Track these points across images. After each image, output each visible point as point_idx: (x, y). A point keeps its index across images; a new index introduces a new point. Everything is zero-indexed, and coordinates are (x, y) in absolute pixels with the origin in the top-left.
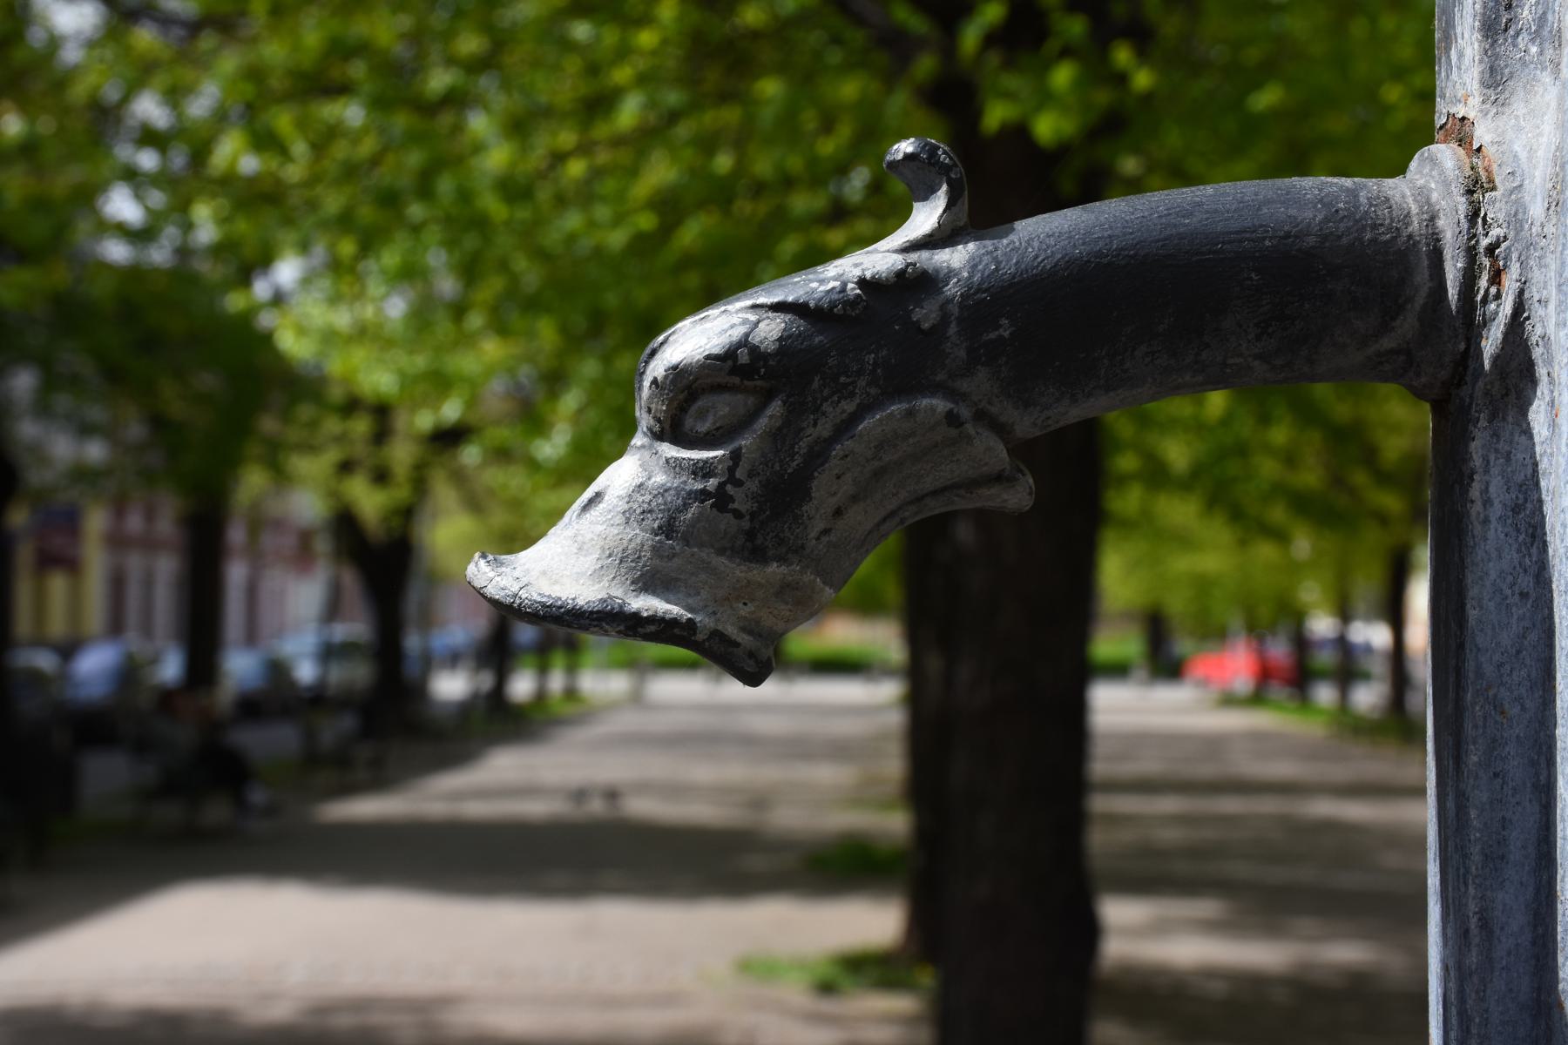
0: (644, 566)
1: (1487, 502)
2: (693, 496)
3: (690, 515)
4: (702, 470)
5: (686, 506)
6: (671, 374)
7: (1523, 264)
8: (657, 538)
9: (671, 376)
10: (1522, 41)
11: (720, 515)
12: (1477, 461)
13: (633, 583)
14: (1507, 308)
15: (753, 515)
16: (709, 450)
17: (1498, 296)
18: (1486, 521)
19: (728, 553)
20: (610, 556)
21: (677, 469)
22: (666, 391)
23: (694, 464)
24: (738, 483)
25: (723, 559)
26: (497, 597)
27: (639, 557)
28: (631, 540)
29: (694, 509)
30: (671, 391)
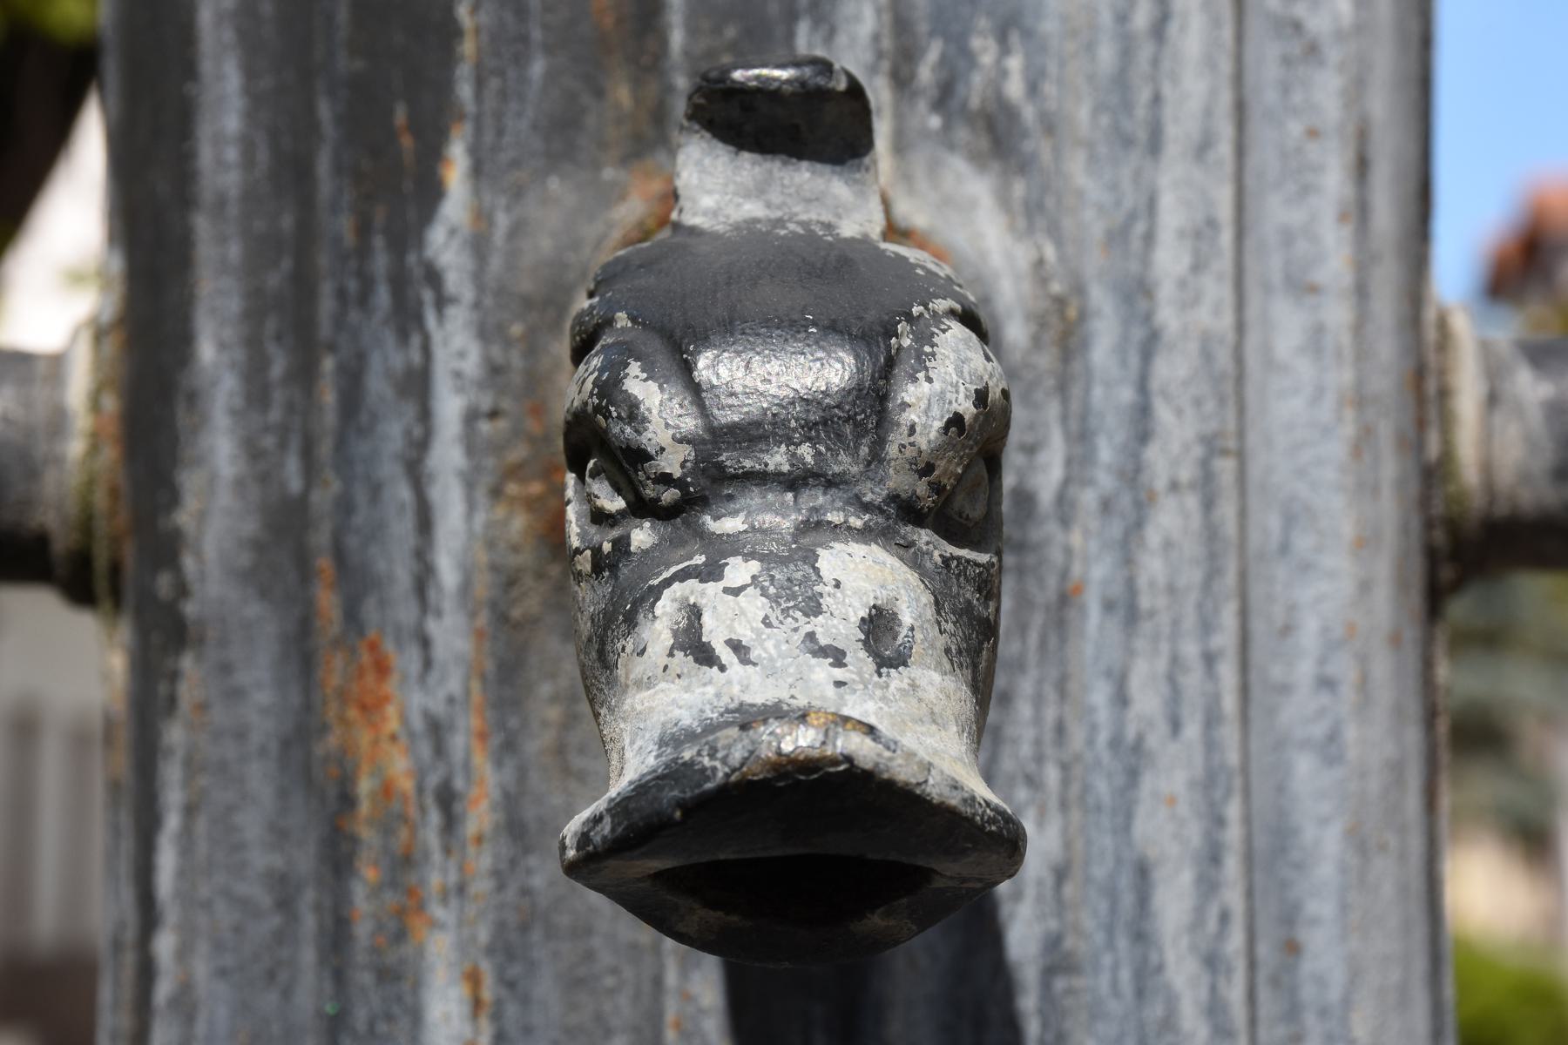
21: (962, 579)
22: (971, 442)
23: (981, 573)
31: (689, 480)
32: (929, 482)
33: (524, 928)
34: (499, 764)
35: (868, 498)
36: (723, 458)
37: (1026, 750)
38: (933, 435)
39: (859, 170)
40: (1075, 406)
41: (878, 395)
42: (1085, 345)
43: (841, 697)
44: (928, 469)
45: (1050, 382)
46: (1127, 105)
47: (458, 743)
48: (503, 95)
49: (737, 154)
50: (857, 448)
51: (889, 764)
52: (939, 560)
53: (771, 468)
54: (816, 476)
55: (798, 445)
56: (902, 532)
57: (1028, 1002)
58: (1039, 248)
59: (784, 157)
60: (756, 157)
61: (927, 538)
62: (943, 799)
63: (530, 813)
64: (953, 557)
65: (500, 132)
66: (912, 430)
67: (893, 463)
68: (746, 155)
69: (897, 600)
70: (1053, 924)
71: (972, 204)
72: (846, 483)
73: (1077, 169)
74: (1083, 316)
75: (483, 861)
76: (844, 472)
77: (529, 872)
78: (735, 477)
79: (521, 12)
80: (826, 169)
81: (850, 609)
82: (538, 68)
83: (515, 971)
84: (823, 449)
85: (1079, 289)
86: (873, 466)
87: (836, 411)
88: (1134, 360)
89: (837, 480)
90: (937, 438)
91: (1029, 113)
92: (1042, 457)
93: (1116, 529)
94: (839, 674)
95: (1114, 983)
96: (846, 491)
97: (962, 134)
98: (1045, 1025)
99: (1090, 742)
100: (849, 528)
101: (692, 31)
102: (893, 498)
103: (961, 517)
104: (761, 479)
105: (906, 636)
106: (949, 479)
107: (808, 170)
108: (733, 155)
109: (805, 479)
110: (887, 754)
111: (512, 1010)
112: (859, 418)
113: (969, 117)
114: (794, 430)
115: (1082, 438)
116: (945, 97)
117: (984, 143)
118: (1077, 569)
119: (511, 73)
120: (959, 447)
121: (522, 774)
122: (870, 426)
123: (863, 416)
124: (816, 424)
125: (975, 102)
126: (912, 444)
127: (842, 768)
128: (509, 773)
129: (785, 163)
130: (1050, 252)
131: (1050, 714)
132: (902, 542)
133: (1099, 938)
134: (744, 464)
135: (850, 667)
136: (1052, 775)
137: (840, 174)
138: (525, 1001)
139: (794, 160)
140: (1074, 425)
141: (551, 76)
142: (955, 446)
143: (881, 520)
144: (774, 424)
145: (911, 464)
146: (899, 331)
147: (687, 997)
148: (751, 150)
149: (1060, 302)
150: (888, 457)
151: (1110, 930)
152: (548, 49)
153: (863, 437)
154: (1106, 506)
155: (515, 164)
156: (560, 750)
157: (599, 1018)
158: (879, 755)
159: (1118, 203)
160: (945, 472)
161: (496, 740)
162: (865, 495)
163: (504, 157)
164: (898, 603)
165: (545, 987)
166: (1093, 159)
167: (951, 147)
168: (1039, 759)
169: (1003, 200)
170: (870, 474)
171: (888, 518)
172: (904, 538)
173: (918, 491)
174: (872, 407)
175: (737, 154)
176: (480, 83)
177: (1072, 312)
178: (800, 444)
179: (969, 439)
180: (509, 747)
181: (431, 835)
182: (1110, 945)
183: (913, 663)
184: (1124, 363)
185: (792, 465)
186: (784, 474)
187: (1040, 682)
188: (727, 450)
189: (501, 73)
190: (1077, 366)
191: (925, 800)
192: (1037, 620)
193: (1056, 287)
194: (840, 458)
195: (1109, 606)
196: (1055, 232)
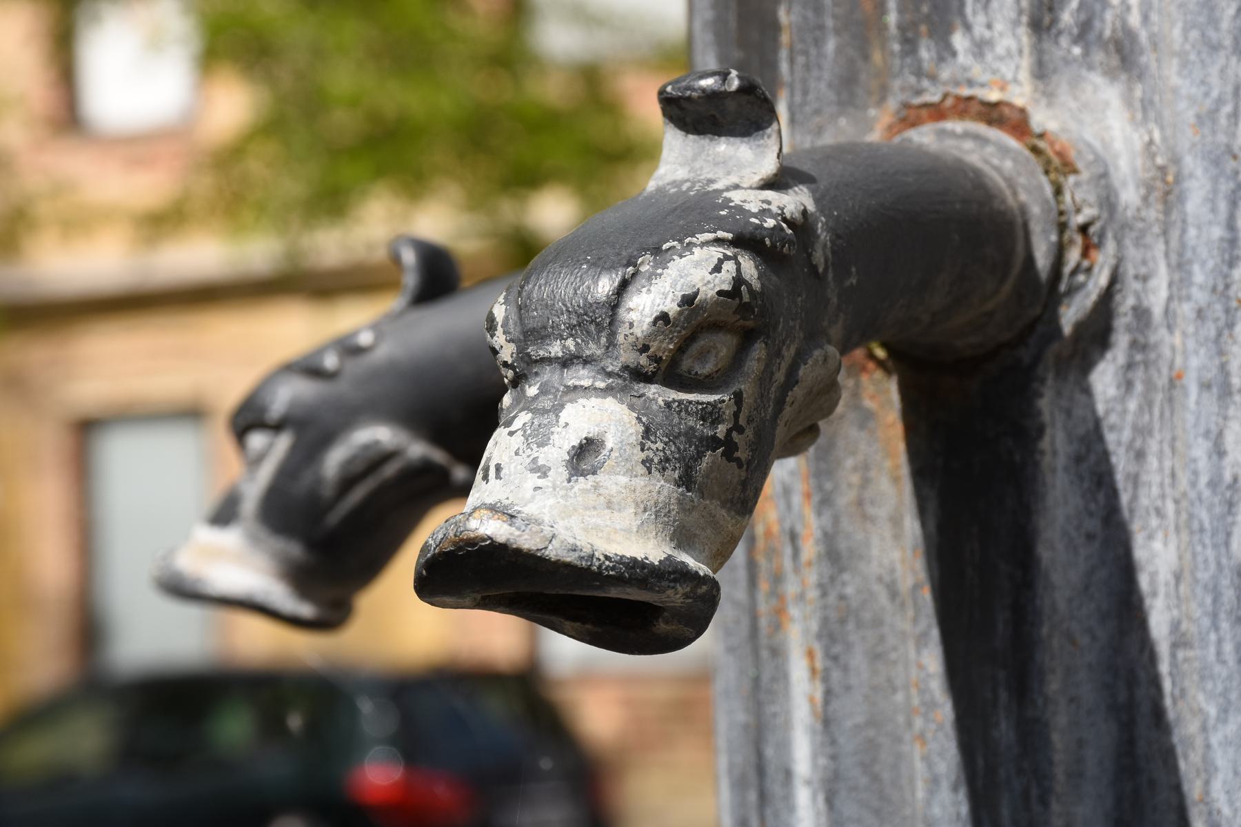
0: (675, 521)
1: (1055, 453)
2: (704, 443)
3: (704, 465)
4: (710, 414)
5: (700, 455)
6: (686, 310)
7: (1119, 242)
8: (680, 490)
9: (687, 312)
10: (1064, 41)
11: (728, 464)
12: (1046, 417)
13: (671, 540)
14: (1103, 279)
15: (749, 463)
16: (711, 394)
17: (1089, 270)
18: (1054, 471)
19: (729, 505)
20: (645, 510)
21: (683, 414)
22: (678, 329)
23: (703, 409)
24: (740, 430)
25: (723, 512)
26: (568, 559)
27: (669, 512)
28: (659, 492)
29: (708, 458)
30: (684, 328)
31: (515, 364)
32: (647, 356)
33: (843, 621)
34: (819, 514)
35: (609, 369)
36: (529, 350)
37: (1155, 490)
38: (645, 327)
39: (763, 138)
40: (1174, 243)
41: (610, 305)
42: (1182, 199)
43: (533, 497)
44: (645, 349)
45: (1156, 229)
46: (1214, 22)
47: (797, 499)
48: (807, 67)
49: (686, 136)
50: (599, 338)
51: (517, 539)
52: (662, 404)
53: (553, 355)
54: (578, 357)
55: (566, 339)
56: (636, 388)
57: (1164, 668)
58: (1150, 133)
59: (710, 136)
60: (695, 137)
61: (655, 391)
62: (559, 558)
63: (842, 545)
64: (674, 401)
65: (805, 92)
66: (631, 325)
67: (622, 347)
68: (691, 137)
69: (606, 432)
70: (1175, 612)
71: (1107, 104)
72: (595, 360)
73: (1172, 74)
74: (1178, 179)
75: (812, 577)
76: (593, 355)
77: (844, 584)
78: (536, 361)
79: (818, 9)
80: (737, 140)
81: (567, 441)
82: (831, 45)
83: (837, 649)
84: (580, 341)
85: (1176, 160)
86: (610, 349)
87: (585, 317)
88: (1223, 206)
89: (589, 359)
90: (648, 329)
91: (1143, 36)
92: (1153, 283)
93: (1211, 330)
94: (540, 482)
95: (1219, 653)
96: (596, 366)
97: (1098, 56)
98: (1174, 684)
99: (1193, 484)
100: (595, 388)
101: (901, 11)
102: (626, 368)
103: (690, 374)
104: (549, 361)
105: (605, 455)
106: (663, 353)
107: (724, 143)
108: (684, 138)
109: (571, 360)
110: (517, 533)
111: (836, 675)
112: (598, 320)
113: (1102, 43)
114: (564, 331)
115: (1181, 267)
116: (1084, 32)
117: (1115, 61)
118: (1179, 361)
119: (813, 51)
120: (667, 332)
121: (836, 520)
122: (605, 325)
123: (600, 319)
124: (575, 326)
125: (1108, 33)
126: (632, 334)
127: (488, 543)
128: (826, 520)
129: (711, 140)
130: (1157, 135)
131: (1168, 464)
132: (635, 394)
133: (1206, 622)
134: (540, 353)
135: (549, 478)
136: (1170, 507)
137: (748, 143)
138: (846, 669)
139: (716, 137)
140: (1174, 258)
141: (839, 50)
142: (663, 332)
143: (620, 381)
144: (552, 327)
145: (633, 346)
146: (638, 262)
147: (921, 667)
148: (693, 133)
149: (1163, 169)
150: (618, 343)
151: (1215, 616)
152: (837, 32)
153: (602, 332)
154: (1200, 314)
155: (817, 112)
156: (860, 503)
157: (889, 680)
158: (511, 534)
159: (1207, 94)
160: (659, 349)
161: (816, 498)
162: (607, 367)
163: (808, 109)
164: (607, 434)
165: (858, 660)
166: (1185, 64)
167: (1090, 68)
168: (1163, 496)
169: (1128, 101)
170: (609, 354)
171: (625, 380)
172: (637, 391)
173: (641, 362)
174: (606, 313)
175: (686, 136)
176: (792, 61)
177: (1170, 178)
178: (567, 339)
179: (677, 327)
180: (825, 502)
181: (787, 563)
182: (1215, 626)
183: (601, 472)
184: (1214, 210)
185: (563, 352)
186: (559, 358)
187: (1161, 442)
188: (531, 345)
189: (805, 53)
190: (1175, 216)
191: (545, 559)
192: (1159, 397)
193: (1160, 161)
194: (589, 346)
195: (1205, 386)
196: (1159, 120)
